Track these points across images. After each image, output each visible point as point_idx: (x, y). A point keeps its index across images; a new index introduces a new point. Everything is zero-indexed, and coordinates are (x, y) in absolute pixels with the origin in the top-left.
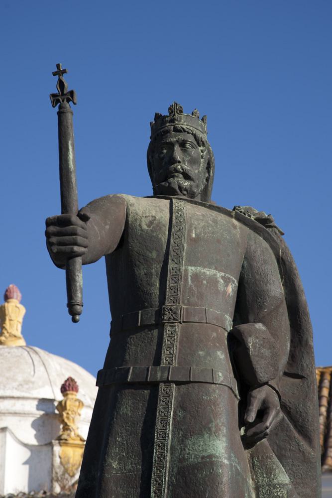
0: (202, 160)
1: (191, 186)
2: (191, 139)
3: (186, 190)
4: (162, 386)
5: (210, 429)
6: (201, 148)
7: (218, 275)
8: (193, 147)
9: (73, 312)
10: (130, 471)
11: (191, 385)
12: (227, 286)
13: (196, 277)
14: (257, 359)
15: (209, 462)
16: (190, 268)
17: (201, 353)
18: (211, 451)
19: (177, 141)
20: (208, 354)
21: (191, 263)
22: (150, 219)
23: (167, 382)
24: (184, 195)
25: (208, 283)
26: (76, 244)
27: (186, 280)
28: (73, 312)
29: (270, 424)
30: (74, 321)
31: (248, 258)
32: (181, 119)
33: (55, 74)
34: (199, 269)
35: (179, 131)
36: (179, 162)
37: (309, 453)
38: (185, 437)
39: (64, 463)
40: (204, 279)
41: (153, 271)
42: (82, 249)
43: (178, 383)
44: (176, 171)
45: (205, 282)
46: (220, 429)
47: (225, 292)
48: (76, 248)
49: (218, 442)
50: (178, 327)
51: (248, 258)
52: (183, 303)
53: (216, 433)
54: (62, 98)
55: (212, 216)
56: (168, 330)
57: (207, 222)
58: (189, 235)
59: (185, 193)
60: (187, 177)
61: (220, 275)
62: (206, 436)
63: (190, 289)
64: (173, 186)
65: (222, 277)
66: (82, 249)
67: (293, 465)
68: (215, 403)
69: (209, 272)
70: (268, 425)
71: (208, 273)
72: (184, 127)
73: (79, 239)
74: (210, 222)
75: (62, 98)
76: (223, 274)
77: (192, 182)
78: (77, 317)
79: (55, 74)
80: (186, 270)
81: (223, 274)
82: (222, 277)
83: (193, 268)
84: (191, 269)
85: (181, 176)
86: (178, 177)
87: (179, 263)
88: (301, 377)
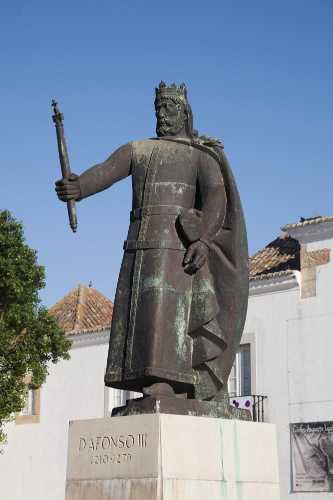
0: (179, 112)
1: (171, 130)
2: (171, 102)
3: (168, 132)
4: (138, 251)
5: (154, 273)
6: (178, 105)
7: (172, 184)
8: (171, 107)
9: (73, 228)
10: (125, 295)
11: (149, 250)
12: (178, 189)
13: (159, 188)
14: (188, 230)
15: (153, 291)
16: (156, 183)
17: (156, 232)
18: (154, 285)
19: (162, 105)
20: (159, 232)
21: (157, 181)
22: (141, 156)
23: (140, 249)
24: (168, 135)
25: (165, 190)
26: (67, 194)
27: (154, 191)
28: (73, 228)
29: (197, 263)
30: (74, 232)
31: (200, 165)
32: (164, 91)
33: (52, 105)
34: (162, 183)
35: (163, 99)
36: (163, 117)
37: (232, 271)
38: (144, 278)
39: (321, 224)
40: (163, 189)
41: (140, 187)
42: (72, 196)
43: (144, 250)
44: (162, 123)
45: (164, 190)
46: (159, 273)
47: (176, 193)
48: (68, 196)
49: (157, 279)
50: (148, 218)
51: (200, 165)
52: (151, 204)
53: (157, 275)
54: (57, 118)
55: (176, 148)
56: (143, 219)
57: (171, 153)
58: (159, 164)
59: (168, 134)
60: (168, 125)
61: (173, 184)
62: (152, 277)
63: (156, 195)
64: (161, 132)
65: (175, 185)
66: (72, 196)
67: (224, 277)
68: (159, 259)
69: (166, 184)
70: (195, 263)
71: (166, 185)
72: (165, 96)
73: (68, 192)
74: (173, 152)
75: (57, 118)
76: (176, 183)
77: (171, 127)
78: (75, 230)
79: (52, 105)
80: (154, 185)
81: (176, 183)
82: (175, 185)
83: (158, 183)
84: (157, 184)
85: (165, 125)
86: (163, 126)
87: (150, 182)
88: (230, 229)
